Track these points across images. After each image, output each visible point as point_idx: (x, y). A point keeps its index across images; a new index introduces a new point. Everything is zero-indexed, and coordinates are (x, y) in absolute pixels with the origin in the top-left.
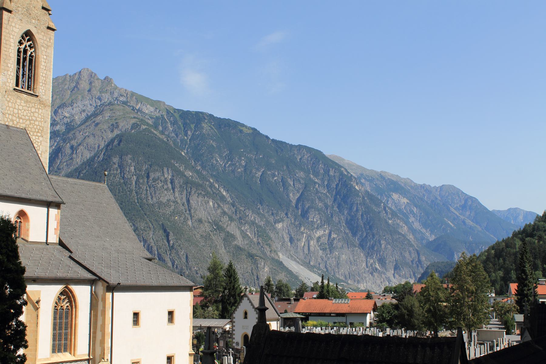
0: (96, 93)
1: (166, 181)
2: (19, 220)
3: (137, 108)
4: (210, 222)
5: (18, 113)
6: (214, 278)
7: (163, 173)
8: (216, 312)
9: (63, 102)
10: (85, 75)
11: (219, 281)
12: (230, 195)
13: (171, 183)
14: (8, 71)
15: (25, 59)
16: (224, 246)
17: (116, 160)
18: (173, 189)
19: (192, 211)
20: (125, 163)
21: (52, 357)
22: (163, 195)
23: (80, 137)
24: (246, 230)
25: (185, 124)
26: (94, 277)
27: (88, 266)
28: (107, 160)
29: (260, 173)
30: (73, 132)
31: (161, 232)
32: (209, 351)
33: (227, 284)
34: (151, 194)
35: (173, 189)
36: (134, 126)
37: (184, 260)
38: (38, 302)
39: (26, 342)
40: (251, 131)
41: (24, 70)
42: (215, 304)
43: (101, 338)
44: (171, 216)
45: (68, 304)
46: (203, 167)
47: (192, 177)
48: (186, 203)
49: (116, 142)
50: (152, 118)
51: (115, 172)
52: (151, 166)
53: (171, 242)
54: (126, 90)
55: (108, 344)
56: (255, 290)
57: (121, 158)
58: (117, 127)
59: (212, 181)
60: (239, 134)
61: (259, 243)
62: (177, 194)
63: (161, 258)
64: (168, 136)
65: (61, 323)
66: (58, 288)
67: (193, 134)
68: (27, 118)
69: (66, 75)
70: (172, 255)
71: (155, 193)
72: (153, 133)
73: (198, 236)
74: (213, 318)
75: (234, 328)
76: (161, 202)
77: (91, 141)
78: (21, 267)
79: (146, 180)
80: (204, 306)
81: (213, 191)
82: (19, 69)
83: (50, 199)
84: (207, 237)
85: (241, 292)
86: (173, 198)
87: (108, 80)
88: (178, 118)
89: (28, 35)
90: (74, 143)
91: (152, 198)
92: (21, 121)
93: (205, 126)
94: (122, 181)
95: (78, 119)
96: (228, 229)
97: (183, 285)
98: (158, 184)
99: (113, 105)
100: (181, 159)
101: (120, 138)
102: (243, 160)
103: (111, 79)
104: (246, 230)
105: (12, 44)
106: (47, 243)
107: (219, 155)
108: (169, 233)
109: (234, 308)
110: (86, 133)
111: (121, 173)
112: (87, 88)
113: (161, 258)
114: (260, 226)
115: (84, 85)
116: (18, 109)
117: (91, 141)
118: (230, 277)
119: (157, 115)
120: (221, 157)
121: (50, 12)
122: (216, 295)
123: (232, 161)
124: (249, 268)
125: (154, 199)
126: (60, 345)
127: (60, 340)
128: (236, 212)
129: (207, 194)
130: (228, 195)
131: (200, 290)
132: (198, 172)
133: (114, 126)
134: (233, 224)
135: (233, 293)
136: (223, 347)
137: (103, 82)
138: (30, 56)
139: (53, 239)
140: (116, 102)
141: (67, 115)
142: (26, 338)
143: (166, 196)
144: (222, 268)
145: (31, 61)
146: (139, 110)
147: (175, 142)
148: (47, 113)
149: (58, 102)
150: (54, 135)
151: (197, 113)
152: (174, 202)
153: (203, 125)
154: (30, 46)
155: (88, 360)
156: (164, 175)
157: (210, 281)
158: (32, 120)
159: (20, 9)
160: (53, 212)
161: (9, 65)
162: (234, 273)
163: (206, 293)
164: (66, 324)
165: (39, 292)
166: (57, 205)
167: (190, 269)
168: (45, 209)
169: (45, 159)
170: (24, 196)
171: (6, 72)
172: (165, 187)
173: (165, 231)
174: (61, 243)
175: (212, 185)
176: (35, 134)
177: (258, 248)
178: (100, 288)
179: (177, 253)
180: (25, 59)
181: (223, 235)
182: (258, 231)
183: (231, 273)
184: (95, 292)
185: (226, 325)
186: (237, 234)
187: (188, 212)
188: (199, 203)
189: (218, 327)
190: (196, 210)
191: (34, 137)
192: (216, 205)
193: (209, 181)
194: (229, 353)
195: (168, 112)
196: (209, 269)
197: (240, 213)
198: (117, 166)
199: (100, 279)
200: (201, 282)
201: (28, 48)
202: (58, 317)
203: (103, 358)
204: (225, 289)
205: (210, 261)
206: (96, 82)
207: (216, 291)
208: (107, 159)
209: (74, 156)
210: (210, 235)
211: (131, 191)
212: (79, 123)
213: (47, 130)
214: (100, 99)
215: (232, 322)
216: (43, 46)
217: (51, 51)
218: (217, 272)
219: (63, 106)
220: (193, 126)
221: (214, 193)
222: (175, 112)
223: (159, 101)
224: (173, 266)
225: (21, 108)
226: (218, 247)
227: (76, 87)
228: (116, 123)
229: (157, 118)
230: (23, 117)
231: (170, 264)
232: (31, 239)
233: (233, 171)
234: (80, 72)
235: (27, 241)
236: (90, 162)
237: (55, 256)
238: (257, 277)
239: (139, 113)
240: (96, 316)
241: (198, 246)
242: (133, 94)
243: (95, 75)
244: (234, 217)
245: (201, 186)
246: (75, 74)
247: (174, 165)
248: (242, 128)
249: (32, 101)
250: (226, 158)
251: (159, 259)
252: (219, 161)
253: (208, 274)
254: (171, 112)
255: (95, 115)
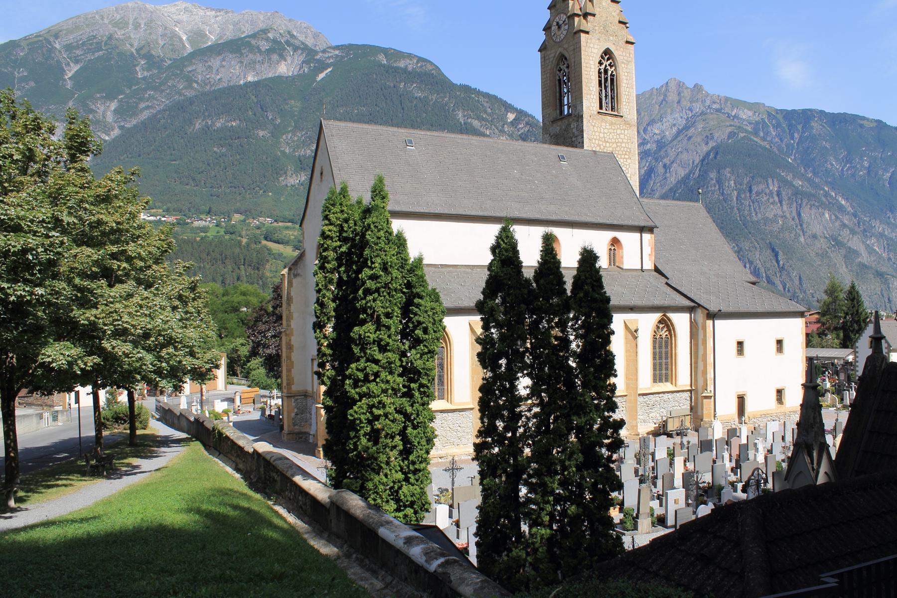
0: (686, 103)
1: (771, 193)
2: (613, 248)
3: (733, 114)
4: (826, 238)
5: (604, 137)
6: (833, 302)
7: (767, 184)
8: (836, 341)
9: (652, 118)
10: (673, 85)
11: (839, 305)
12: (851, 204)
13: (778, 195)
14: (590, 94)
15: (606, 79)
16: (845, 264)
17: (713, 175)
18: (781, 202)
19: (805, 226)
20: (723, 178)
21: (653, 386)
22: (769, 210)
23: (672, 153)
24: (873, 244)
25: (790, 126)
26: (692, 304)
27: (685, 293)
28: (703, 176)
29: (889, 175)
30: (664, 150)
31: (769, 251)
32: (811, 385)
33: (848, 308)
34: (755, 210)
35: (781, 202)
36: (731, 135)
37: (797, 282)
38: (636, 331)
39: (615, 371)
40: (875, 124)
41: (606, 91)
42: (835, 332)
43: (869, 352)
44: (779, 232)
45: (667, 333)
46: (815, 174)
47: (802, 186)
48: (796, 217)
49: (712, 156)
50: (750, 123)
51: (713, 188)
52: (753, 178)
53: (781, 263)
54: (719, 96)
55: (710, 375)
56: (885, 314)
57: (719, 172)
58: (712, 138)
59: (826, 189)
60: (859, 130)
61: (889, 259)
62: (785, 208)
63: (769, 281)
64: (771, 142)
65: (660, 353)
66: (656, 316)
67: (801, 137)
68: (613, 140)
69: (652, 89)
70: (783, 277)
71: (760, 208)
72: (753, 141)
73: (813, 254)
74: (833, 347)
75: (857, 359)
76: (767, 218)
77: (684, 156)
78: (607, 297)
79: (748, 195)
80: (821, 334)
81: (828, 201)
82: (601, 90)
83: (642, 224)
84: (823, 255)
85: (867, 318)
86: (781, 213)
87: (698, 88)
88: (782, 120)
89: (608, 54)
90: (666, 161)
91: (756, 214)
92: (608, 144)
93: (815, 125)
94: (721, 198)
95: (669, 134)
96: (849, 244)
97: (793, 310)
98: (762, 197)
99: (706, 114)
100: (788, 167)
101: (716, 150)
102: (866, 160)
103: (701, 86)
104: (873, 244)
105: (592, 66)
106: (642, 270)
107: (835, 158)
108: (778, 252)
109: (857, 335)
110: (678, 149)
111: (719, 189)
112: (676, 99)
113: (769, 281)
114: (891, 239)
115: (672, 97)
116: (604, 133)
117: (684, 156)
118: (852, 300)
119: (757, 120)
120: (836, 159)
121: (627, 25)
122: (835, 322)
123: (851, 163)
124: (877, 289)
125: (759, 215)
126: (661, 375)
127: (661, 370)
128: (859, 223)
129: (822, 205)
130: (848, 204)
131: (816, 316)
132: (809, 180)
133: (708, 138)
134: (855, 238)
135: (856, 319)
136: (844, 380)
137: (692, 90)
138: (611, 75)
139: (649, 265)
140: (708, 111)
141: (657, 132)
142: (615, 367)
143: (772, 211)
144: (841, 290)
145: (612, 80)
146: (735, 117)
147: (779, 148)
148: (633, 133)
149: (646, 119)
150: (643, 155)
151: (804, 111)
152: (782, 217)
153: (813, 124)
154: (609, 65)
155: (691, 391)
156: (768, 187)
157: (828, 305)
158: (618, 142)
159: (597, 28)
160: (647, 237)
161: (591, 89)
162: (858, 296)
163: (824, 319)
164: (666, 353)
165: (636, 321)
166: (650, 230)
167: (805, 292)
168: (638, 235)
169: (635, 182)
170: (615, 222)
171: (588, 96)
172: (771, 200)
173: (773, 250)
174: (657, 270)
175: (827, 195)
176: (623, 156)
177: (889, 265)
178: (700, 315)
179: (788, 274)
180: (606, 79)
181: (843, 251)
182: (888, 244)
183: (853, 296)
184: (694, 320)
185: (848, 355)
186: (861, 249)
187: (799, 227)
188: (813, 216)
189: (838, 358)
190: (809, 224)
191: (622, 161)
192: (833, 217)
193: (824, 190)
194: (851, 388)
195: (769, 114)
196: (826, 292)
197: (864, 224)
198: (714, 182)
199: (699, 305)
200: (817, 307)
201: (608, 67)
202: (657, 346)
203: (706, 390)
204: (847, 314)
205: (827, 282)
206: (685, 91)
207: (835, 317)
208: (703, 175)
209: (668, 175)
210: (827, 252)
211: (732, 208)
212: (670, 139)
213: (634, 151)
214: (690, 110)
215: (855, 353)
216: (623, 63)
217: (632, 66)
218: (836, 294)
219: (652, 122)
220: (800, 127)
221: (830, 203)
222: (777, 113)
223: (758, 103)
224: (784, 289)
225: (606, 131)
226: (838, 265)
227: (664, 100)
228: (711, 134)
229: (757, 123)
230: (610, 141)
231: (780, 287)
232: (625, 267)
233: (853, 175)
234: (667, 83)
235: (622, 269)
236: (684, 180)
237: (651, 283)
238: (889, 299)
239: (735, 120)
240: (697, 345)
241: (813, 266)
242: (727, 99)
243: (684, 83)
244: (856, 229)
245: (814, 196)
246: (662, 86)
247: (780, 174)
248: (862, 122)
249: (618, 122)
250: (843, 160)
251: (768, 282)
252: (834, 165)
253: (825, 297)
254: (772, 114)
255: (687, 128)
